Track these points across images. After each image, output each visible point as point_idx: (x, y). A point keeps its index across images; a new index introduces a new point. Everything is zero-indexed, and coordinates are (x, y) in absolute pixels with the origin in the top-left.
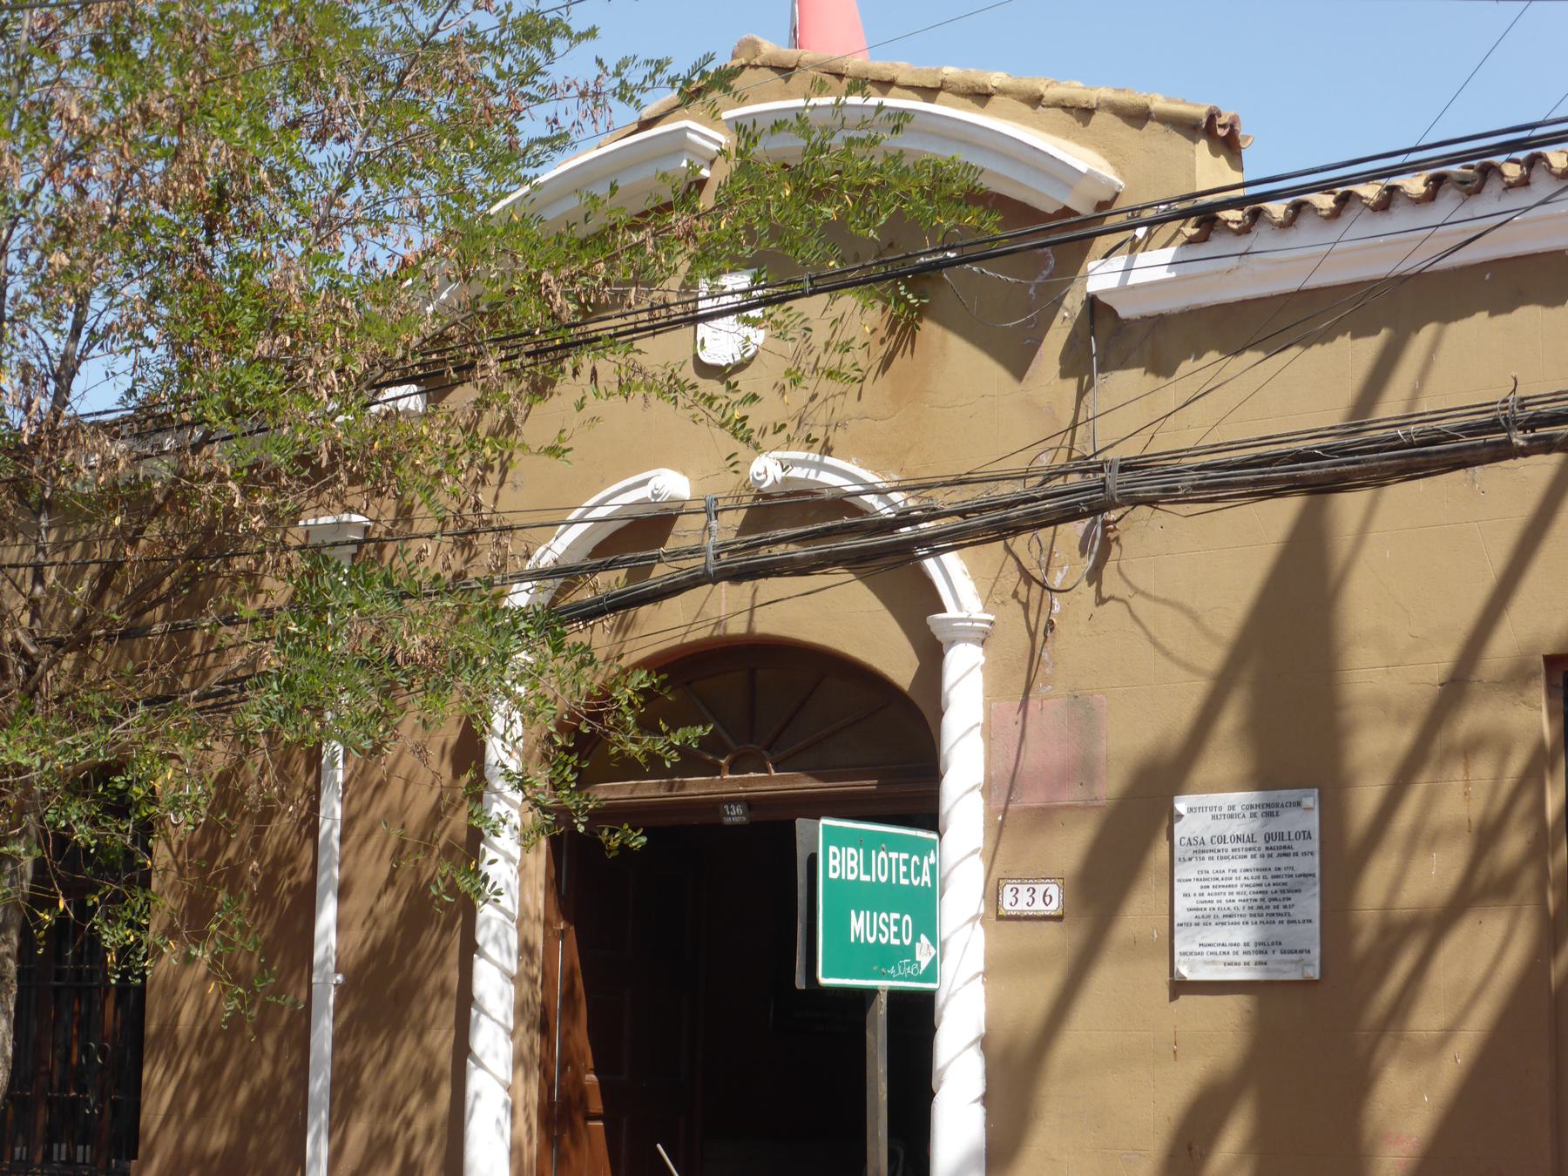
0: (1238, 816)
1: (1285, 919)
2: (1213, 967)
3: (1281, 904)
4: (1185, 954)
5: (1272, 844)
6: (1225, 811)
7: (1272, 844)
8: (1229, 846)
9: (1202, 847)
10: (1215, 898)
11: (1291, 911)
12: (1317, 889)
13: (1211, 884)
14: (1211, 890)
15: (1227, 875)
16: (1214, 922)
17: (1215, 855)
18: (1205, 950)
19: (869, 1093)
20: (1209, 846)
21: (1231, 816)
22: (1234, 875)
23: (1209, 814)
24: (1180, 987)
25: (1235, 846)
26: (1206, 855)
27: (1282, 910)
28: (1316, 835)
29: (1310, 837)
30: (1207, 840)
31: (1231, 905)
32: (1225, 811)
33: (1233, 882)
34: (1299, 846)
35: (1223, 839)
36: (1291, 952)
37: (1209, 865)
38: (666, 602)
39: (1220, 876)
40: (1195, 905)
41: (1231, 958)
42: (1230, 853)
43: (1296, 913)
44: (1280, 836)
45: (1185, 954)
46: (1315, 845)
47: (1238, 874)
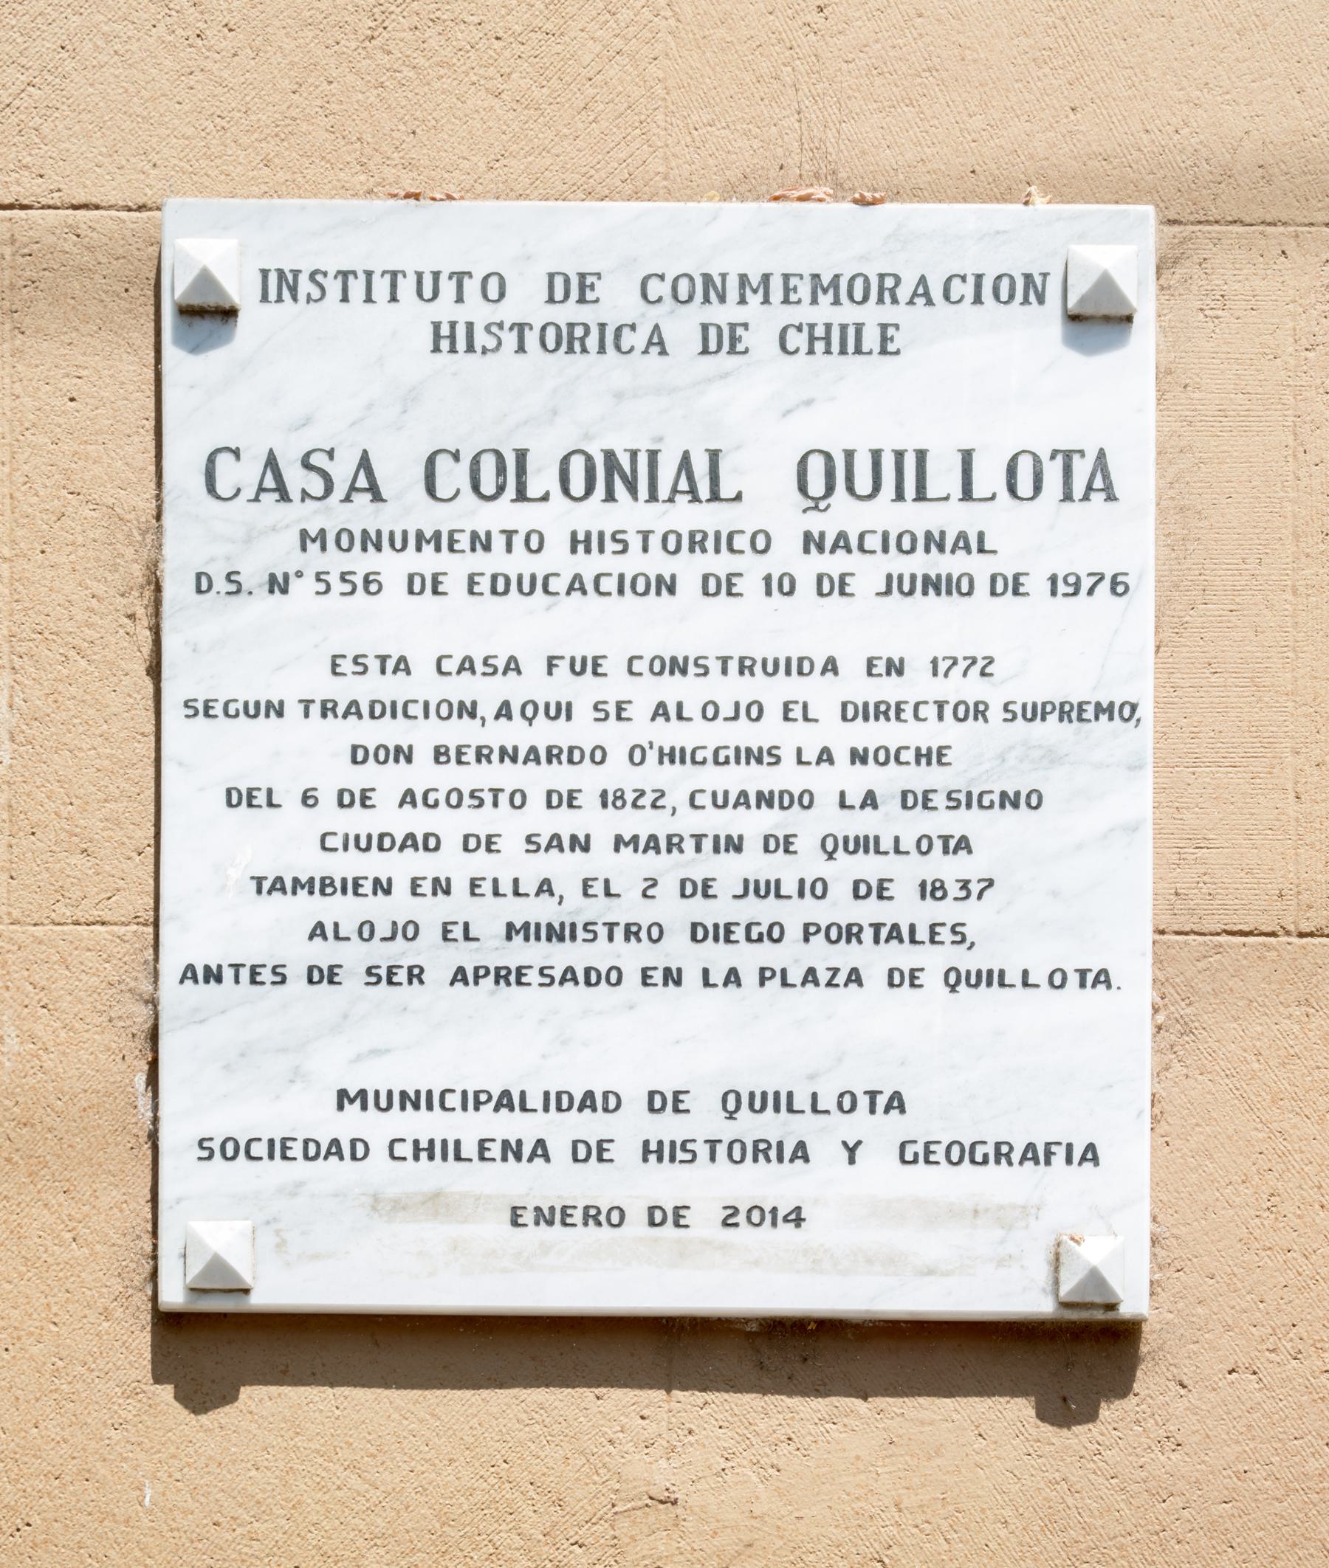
0: (612, 339)
1: (933, 961)
2: (435, 1233)
3: (906, 873)
4: (234, 1149)
5: (844, 514)
6: (526, 302)
7: (844, 514)
8: (557, 518)
9: (361, 515)
10: (450, 824)
11: (973, 915)
12: (1138, 799)
13: (424, 736)
14: (422, 774)
15: (533, 685)
16: (442, 961)
17: (456, 567)
18: (377, 1128)
19: (985, 1318)
20: (407, 508)
21: (569, 340)
22: (584, 692)
23: (413, 319)
24: (214, 1345)
25: (594, 515)
26: (392, 567)
27: (906, 908)
28: (1137, 476)
29: (1103, 484)
30: (401, 474)
31: (565, 869)
32: (526, 302)
33: (581, 731)
34: (1029, 535)
35: (512, 475)
36: (967, 1154)
37: (393, 621)
38: (153, 324)
39: (488, 692)
40: (315, 864)
41: (559, 1181)
42: (557, 559)
43: (997, 933)
44: (908, 474)
45: (234, 1149)
46: (1123, 535)
47: (614, 687)
